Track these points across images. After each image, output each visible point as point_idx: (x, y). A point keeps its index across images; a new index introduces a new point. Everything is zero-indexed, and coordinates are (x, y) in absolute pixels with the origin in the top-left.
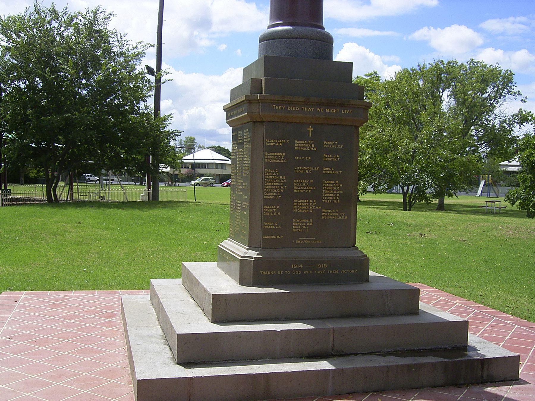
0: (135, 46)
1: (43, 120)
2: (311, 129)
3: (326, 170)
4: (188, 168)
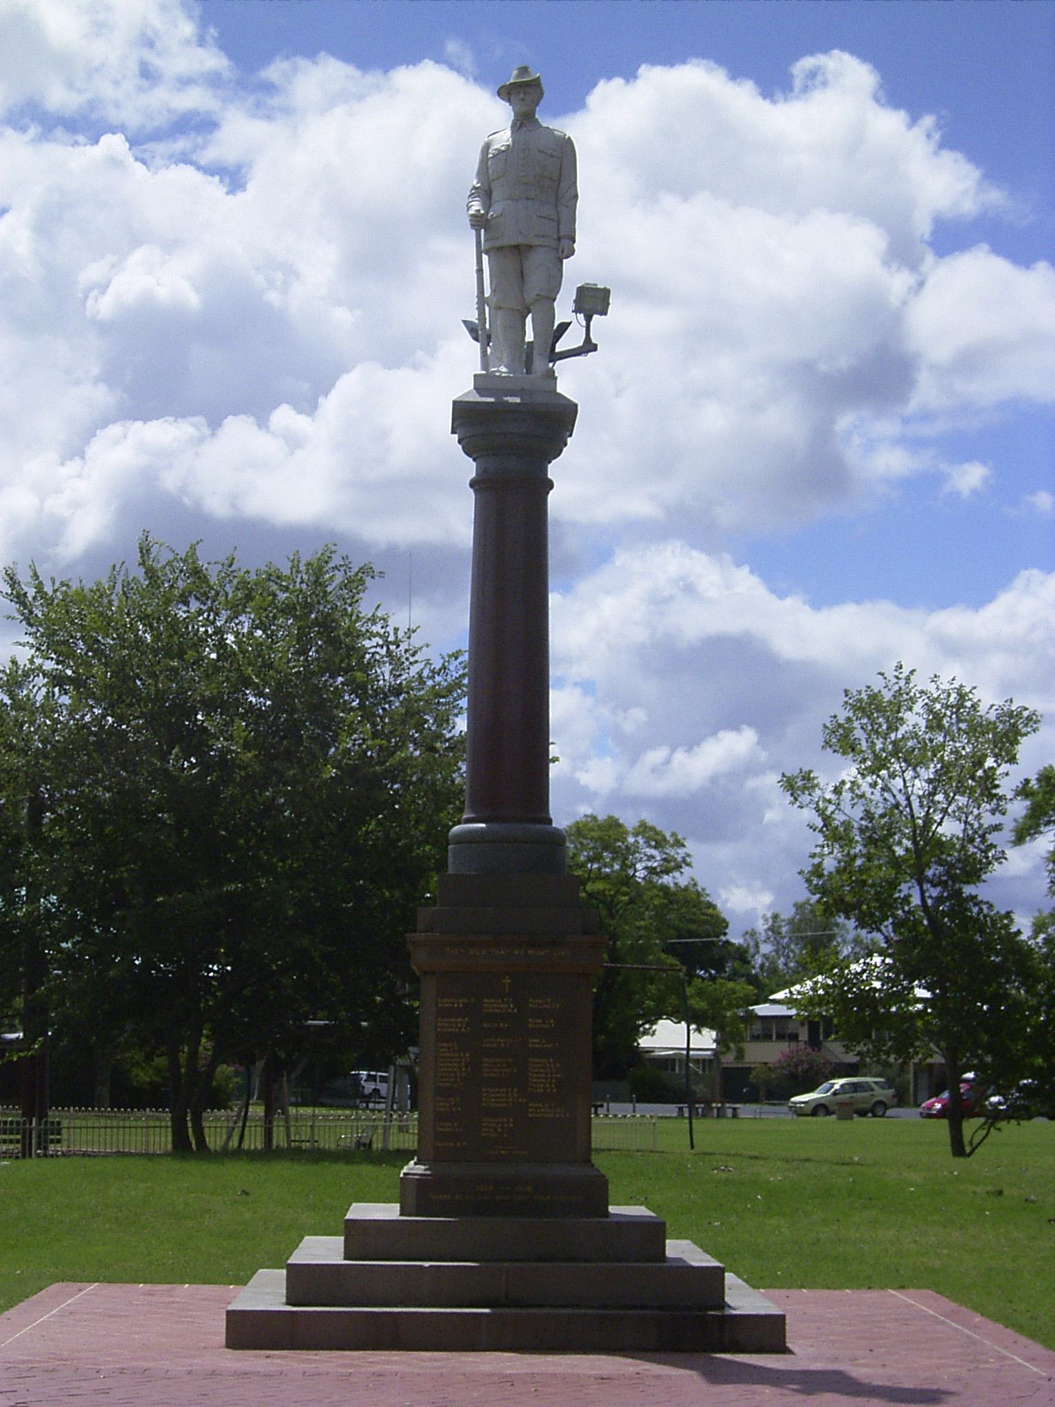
0: (437, 665)
1: (162, 904)
2: (508, 981)
3: (534, 1042)
4: (794, 1037)
